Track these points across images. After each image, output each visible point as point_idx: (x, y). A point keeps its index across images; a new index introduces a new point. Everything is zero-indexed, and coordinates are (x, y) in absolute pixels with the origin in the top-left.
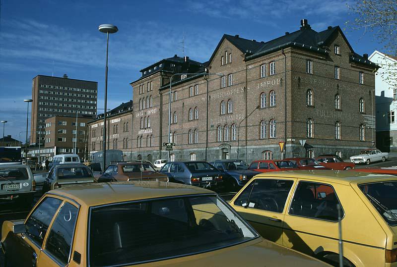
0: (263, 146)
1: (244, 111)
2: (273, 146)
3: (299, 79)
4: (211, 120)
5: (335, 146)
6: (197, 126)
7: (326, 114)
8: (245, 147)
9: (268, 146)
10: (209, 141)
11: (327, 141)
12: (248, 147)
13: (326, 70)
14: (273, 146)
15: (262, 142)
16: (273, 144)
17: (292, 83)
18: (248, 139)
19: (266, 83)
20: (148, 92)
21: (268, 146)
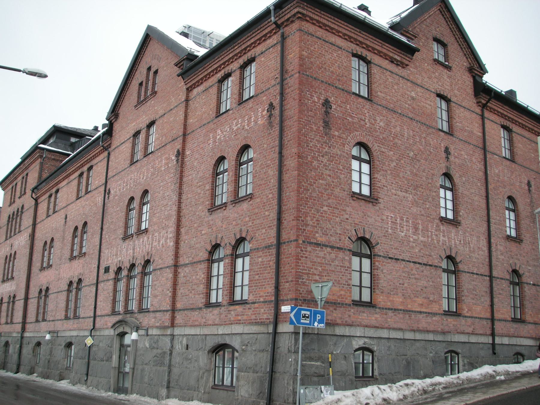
0: (213, 330)
1: (174, 219)
2: (238, 329)
3: (327, 103)
4: (106, 252)
5: (444, 333)
6: (82, 271)
7: (416, 229)
8: (169, 332)
9: (226, 330)
10: (98, 313)
11: (421, 316)
12: (177, 331)
13: (413, 99)
14: (238, 329)
15: (212, 315)
16: (238, 322)
17: (300, 112)
18: (179, 305)
19: (230, 127)
20: (213, 208)
21: (226, 330)
